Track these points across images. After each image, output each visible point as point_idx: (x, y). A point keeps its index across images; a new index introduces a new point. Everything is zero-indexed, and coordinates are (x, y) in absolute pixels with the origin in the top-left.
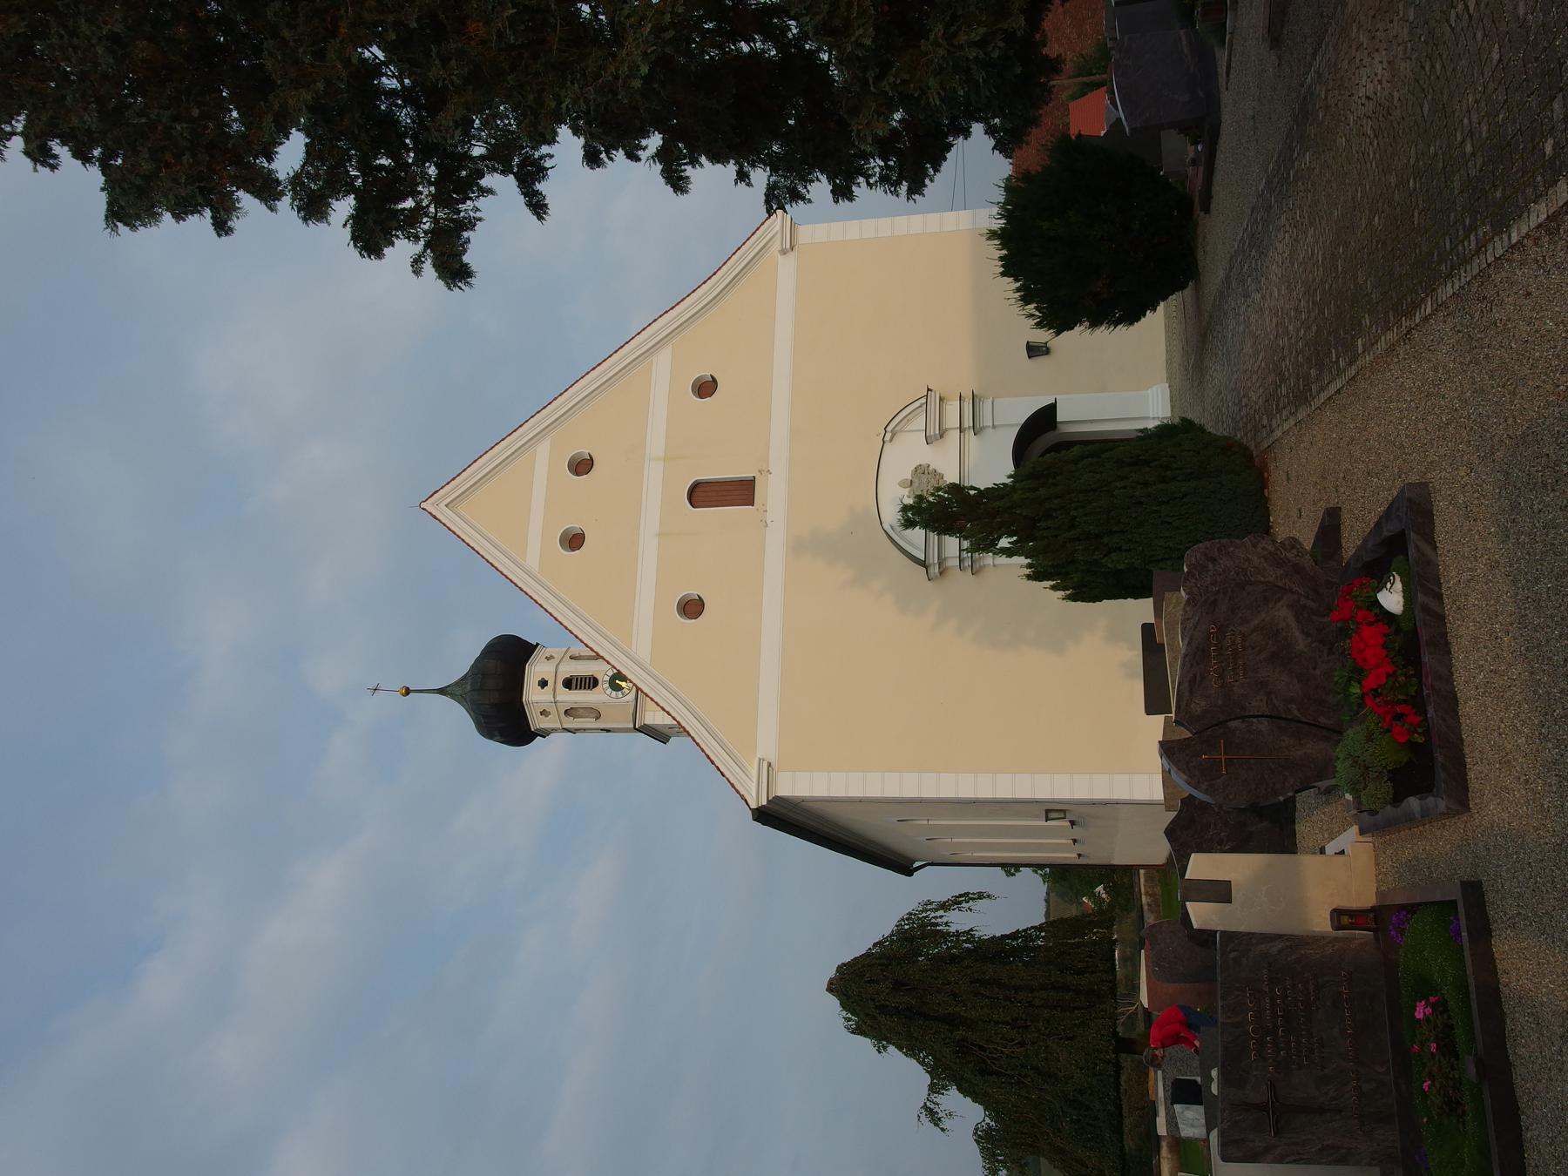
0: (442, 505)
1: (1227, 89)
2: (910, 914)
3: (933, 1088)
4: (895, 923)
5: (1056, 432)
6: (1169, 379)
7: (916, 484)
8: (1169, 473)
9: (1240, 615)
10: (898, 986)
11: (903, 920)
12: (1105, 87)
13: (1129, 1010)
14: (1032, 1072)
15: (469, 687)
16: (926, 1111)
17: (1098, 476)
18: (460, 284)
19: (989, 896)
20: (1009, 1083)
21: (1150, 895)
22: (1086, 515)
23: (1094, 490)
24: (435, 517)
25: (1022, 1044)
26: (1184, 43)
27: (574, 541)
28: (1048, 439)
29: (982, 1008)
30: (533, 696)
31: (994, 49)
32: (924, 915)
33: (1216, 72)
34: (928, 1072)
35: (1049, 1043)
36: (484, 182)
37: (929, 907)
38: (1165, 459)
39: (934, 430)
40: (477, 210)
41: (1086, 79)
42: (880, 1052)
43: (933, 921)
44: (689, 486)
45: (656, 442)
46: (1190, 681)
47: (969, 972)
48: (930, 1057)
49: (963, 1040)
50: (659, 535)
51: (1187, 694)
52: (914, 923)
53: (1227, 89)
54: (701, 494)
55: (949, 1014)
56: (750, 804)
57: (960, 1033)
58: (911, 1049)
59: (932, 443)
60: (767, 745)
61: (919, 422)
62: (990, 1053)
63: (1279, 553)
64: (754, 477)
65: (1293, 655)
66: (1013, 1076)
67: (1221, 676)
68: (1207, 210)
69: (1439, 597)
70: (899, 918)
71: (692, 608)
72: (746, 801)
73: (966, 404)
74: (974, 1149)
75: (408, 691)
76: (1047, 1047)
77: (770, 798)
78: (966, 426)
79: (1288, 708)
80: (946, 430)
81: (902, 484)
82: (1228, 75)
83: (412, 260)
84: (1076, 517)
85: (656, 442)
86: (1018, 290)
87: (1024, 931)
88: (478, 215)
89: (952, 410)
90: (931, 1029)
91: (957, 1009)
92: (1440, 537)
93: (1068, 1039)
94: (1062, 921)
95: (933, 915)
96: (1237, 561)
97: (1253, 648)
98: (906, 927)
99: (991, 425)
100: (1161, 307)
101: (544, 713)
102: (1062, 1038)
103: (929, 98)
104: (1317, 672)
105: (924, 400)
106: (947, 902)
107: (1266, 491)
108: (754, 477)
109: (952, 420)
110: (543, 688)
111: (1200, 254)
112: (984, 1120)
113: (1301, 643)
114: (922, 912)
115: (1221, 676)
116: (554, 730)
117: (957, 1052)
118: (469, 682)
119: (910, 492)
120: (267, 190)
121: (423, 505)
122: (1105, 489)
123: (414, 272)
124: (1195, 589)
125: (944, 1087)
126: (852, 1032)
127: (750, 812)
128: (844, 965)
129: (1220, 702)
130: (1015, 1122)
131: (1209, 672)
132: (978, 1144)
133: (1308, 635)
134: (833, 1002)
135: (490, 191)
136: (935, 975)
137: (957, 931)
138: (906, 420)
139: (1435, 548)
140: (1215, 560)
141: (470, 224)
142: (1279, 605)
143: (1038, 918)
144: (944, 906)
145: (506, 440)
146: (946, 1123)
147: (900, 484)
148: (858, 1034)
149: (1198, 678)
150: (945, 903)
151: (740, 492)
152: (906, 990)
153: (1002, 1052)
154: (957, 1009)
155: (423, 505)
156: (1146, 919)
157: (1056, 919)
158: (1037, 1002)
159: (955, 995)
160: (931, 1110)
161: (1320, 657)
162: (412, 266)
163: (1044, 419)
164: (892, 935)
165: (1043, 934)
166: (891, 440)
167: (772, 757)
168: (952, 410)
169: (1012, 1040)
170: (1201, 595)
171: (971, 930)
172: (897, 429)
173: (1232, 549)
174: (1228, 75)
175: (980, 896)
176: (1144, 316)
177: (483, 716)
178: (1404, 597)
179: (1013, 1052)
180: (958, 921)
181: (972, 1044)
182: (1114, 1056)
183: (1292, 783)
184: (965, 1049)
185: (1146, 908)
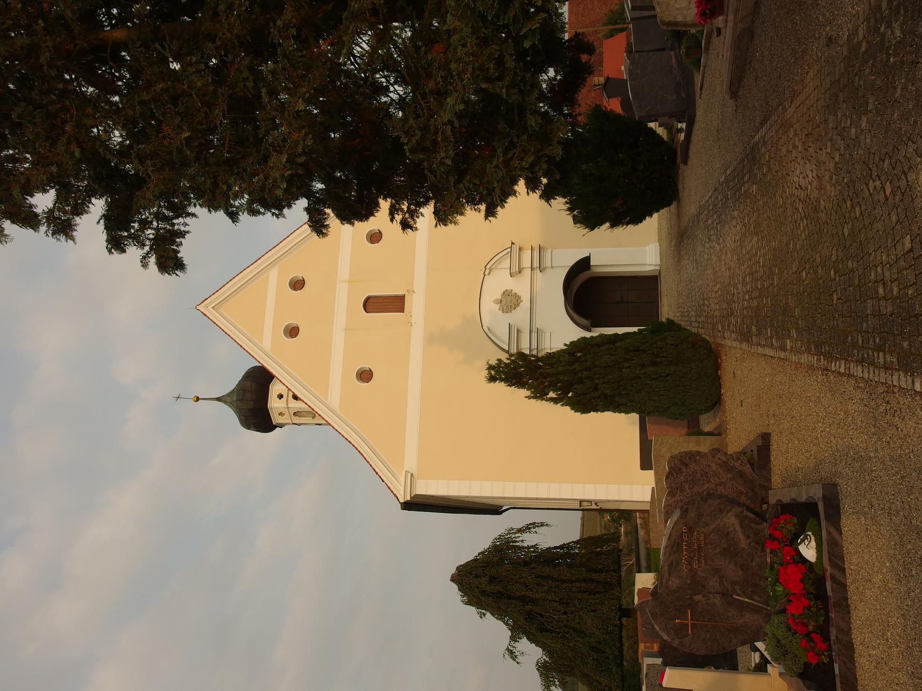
0: (210, 308)
1: (700, 98)
2: (500, 536)
3: (514, 638)
4: (491, 541)
5: (590, 271)
6: (659, 240)
7: (504, 302)
8: (658, 360)
9: (703, 520)
10: (492, 579)
11: (496, 539)
12: (625, 32)
13: (628, 564)
14: (571, 630)
15: (235, 398)
16: (508, 651)
17: (613, 358)
18: (176, 272)
19: (547, 525)
20: (557, 637)
21: (642, 519)
22: (604, 383)
23: (609, 366)
24: (205, 315)
25: (565, 613)
26: (674, 60)
27: (293, 332)
28: (585, 276)
29: (542, 592)
30: (274, 404)
31: (539, 169)
32: (509, 536)
33: (694, 81)
34: (509, 629)
35: (581, 614)
36: (191, 210)
37: (512, 532)
38: (655, 350)
39: (515, 269)
40: (187, 225)
41: (613, 27)
42: (481, 617)
43: (514, 539)
44: (363, 302)
45: (344, 271)
46: (669, 566)
47: (534, 571)
48: (511, 621)
49: (530, 611)
50: (345, 330)
51: (667, 574)
52: (502, 541)
53: (700, 98)
54: (372, 304)
55: (523, 596)
56: (400, 499)
57: (529, 607)
58: (500, 614)
59: (514, 276)
60: (411, 462)
61: (506, 264)
62: (546, 618)
63: (729, 462)
64: (404, 295)
65: (738, 551)
66: (559, 633)
67: (690, 564)
68: (686, 163)
69: (843, 570)
70: (494, 538)
71: (365, 376)
72: (397, 498)
73: (535, 252)
74: (537, 674)
75: (198, 399)
76: (579, 616)
77: (412, 496)
78: (535, 266)
79: (733, 588)
80: (523, 268)
81: (496, 302)
82: (701, 90)
83: (141, 257)
84: (598, 384)
85: (344, 271)
86: (567, 203)
87: (568, 544)
88: (187, 229)
89: (527, 256)
90: (512, 605)
91: (527, 593)
92: (845, 529)
93: (592, 611)
94: (590, 538)
95: (513, 536)
96: (701, 467)
97: (711, 544)
98: (498, 543)
99: (550, 266)
100: (655, 215)
101: (281, 414)
102: (588, 611)
103: (493, 198)
104: (754, 564)
105: (509, 250)
106: (523, 528)
107: (719, 371)
108: (404, 295)
109: (526, 263)
110: (280, 399)
111: (680, 187)
112: (542, 657)
113: (744, 543)
114: (508, 534)
115: (690, 564)
116: (288, 424)
117: (527, 618)
118: (235, 395)
119: (500, 307)
120: (29, 220)
121: (198, 307)
122: (617, 366)
123: (143, 266)
124: (673, 485)
125: (520, 638)
126: (465, 604)
127: (400, 505)
128: (461, 566)
129: (689, 582)
130: (560, 658)
131: (682, 559)
132: (538, 671)
133: (748, 537)
134: (455, 587)
135: (194, 215)
136: (514, 573)
137: (528, 546)
138: (498, 262)
139: (841, 534)
140: (687, 465)
141: (182, 234)
142: (729, 514)
143: (576, 536)
144: (520, 531)
145: (250, 267)
146: (520, 659)
147: (494, 302)
148: (469, 605)
149: (674, 563)
150: (521, 529)
151: (396, 304)
152: (498, 581)
153: (553, 618)
154: (527, 593)
155: (198, 307)
156: (639, 532)
157: (586, 537)
158: (574, 589)
159: (525, 584)
160: (511, 651)
161: (756, 553)
162: (142, 262)
163: (584, 264)
164: (489, 548)
165: (578, 546)
166: (489, 274)
167: (414, 471)
168: (527, 256)
169: (560, 611)
170: (677, 489)
171: (536, 545)
172: (492, 267)
173: (698, 458)
174: (701, 90)
175: (542, 525)
176: (645, 219)
177: (244, 416)
178: (817, 553)
179: (560, 618)
180: (529, 540)
181: (536, 613)
182: (619, 622)
183: (735, 643)
184: (531, 616)
185: (639, 526)
